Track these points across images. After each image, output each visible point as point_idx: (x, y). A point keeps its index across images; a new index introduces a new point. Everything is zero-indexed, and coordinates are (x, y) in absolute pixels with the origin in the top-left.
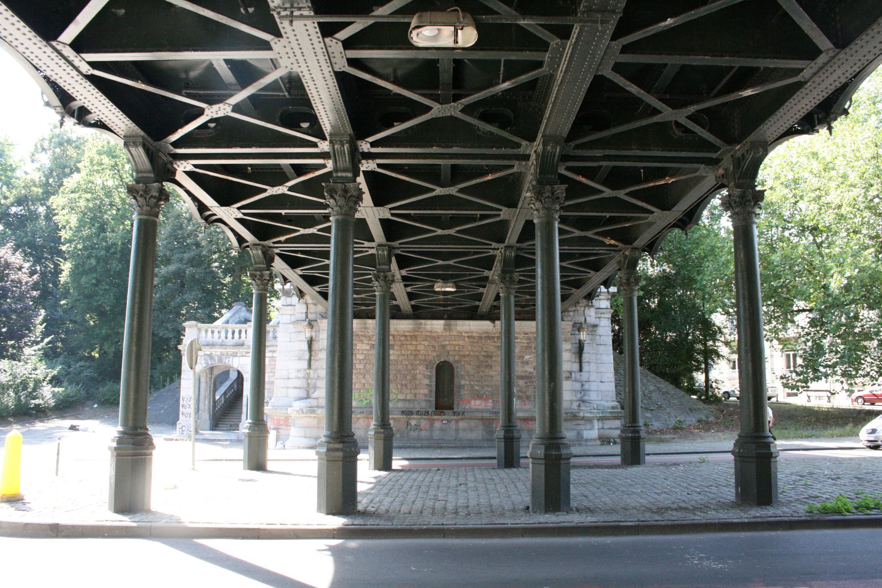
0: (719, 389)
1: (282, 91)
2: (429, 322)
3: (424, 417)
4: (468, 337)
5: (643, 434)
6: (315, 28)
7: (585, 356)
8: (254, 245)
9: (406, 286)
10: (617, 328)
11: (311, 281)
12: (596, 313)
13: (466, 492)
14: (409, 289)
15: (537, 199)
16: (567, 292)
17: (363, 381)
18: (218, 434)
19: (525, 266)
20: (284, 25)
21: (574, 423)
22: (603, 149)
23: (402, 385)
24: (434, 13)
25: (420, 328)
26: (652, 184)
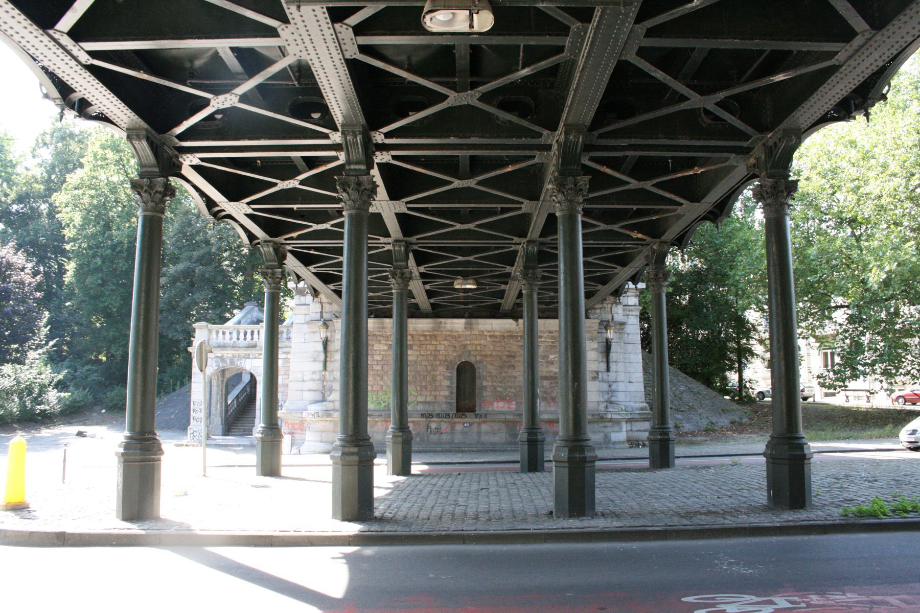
0: (753, 389)
1: (290, 79)
2: (449, 321)
3: (445, 420)
4: (490, 336)
5: (672, 436)
6: (324, 13)
7: (613, 356)
8: (265, 241)
9: (424, 283)
10: (646, 325)
11: (326, 278)
12: (624, 310)
13: (488, 497)
14: (428, 287)
15: (559, 191)
16: (591, 289)
17: (381, 383)
18: (231, 439)
21: (601, 425)
23: (421, 386)
26: (680, 175)
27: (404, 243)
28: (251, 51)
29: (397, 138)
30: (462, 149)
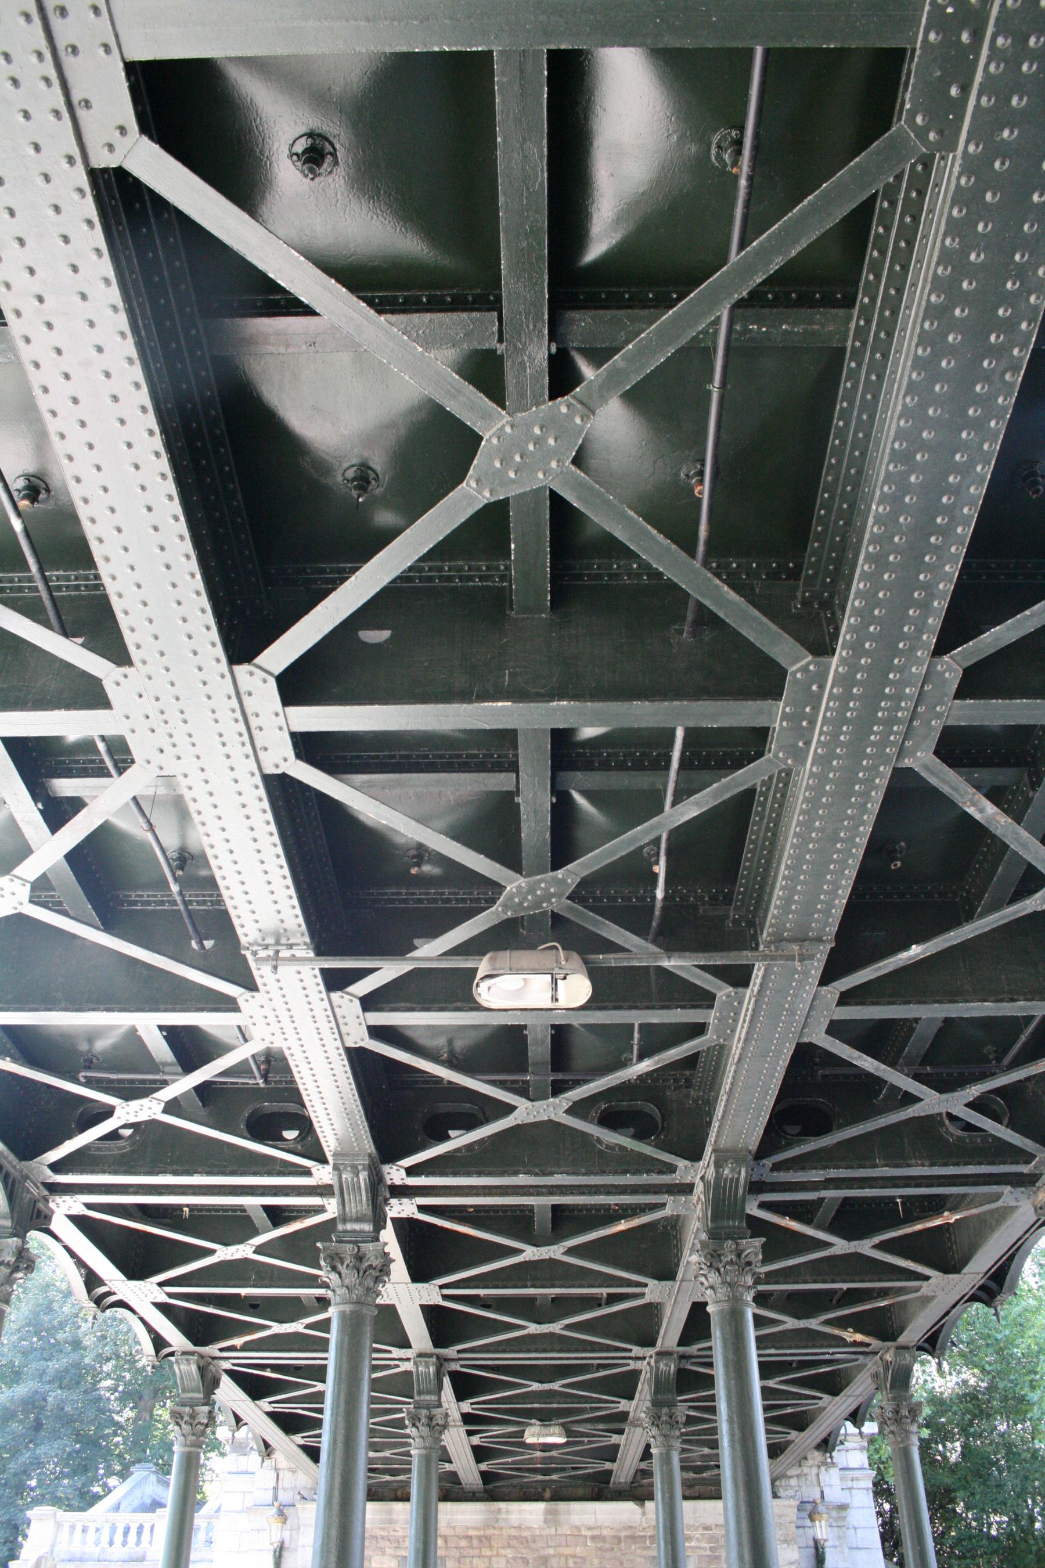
2: (515, 1506)
4: (593, 1538)
6: (316, 977)
8: (184, 1353)
9: (470, 1433)
10: (887, 1506)
11: (288, 1423)
12: (842, 1479)
14: (476, 1440)
15: (711, 1266)
16: (779, 1439)
19: (697, 1390)
20: (261, 973)
22: (824, 1168)
24: (516, 954)
25: (497, 1520)
26: (919, 1227)
27: (434, 1359)
28: (192, 1031)
29: (427, 1175)
30: (538, 1194)
